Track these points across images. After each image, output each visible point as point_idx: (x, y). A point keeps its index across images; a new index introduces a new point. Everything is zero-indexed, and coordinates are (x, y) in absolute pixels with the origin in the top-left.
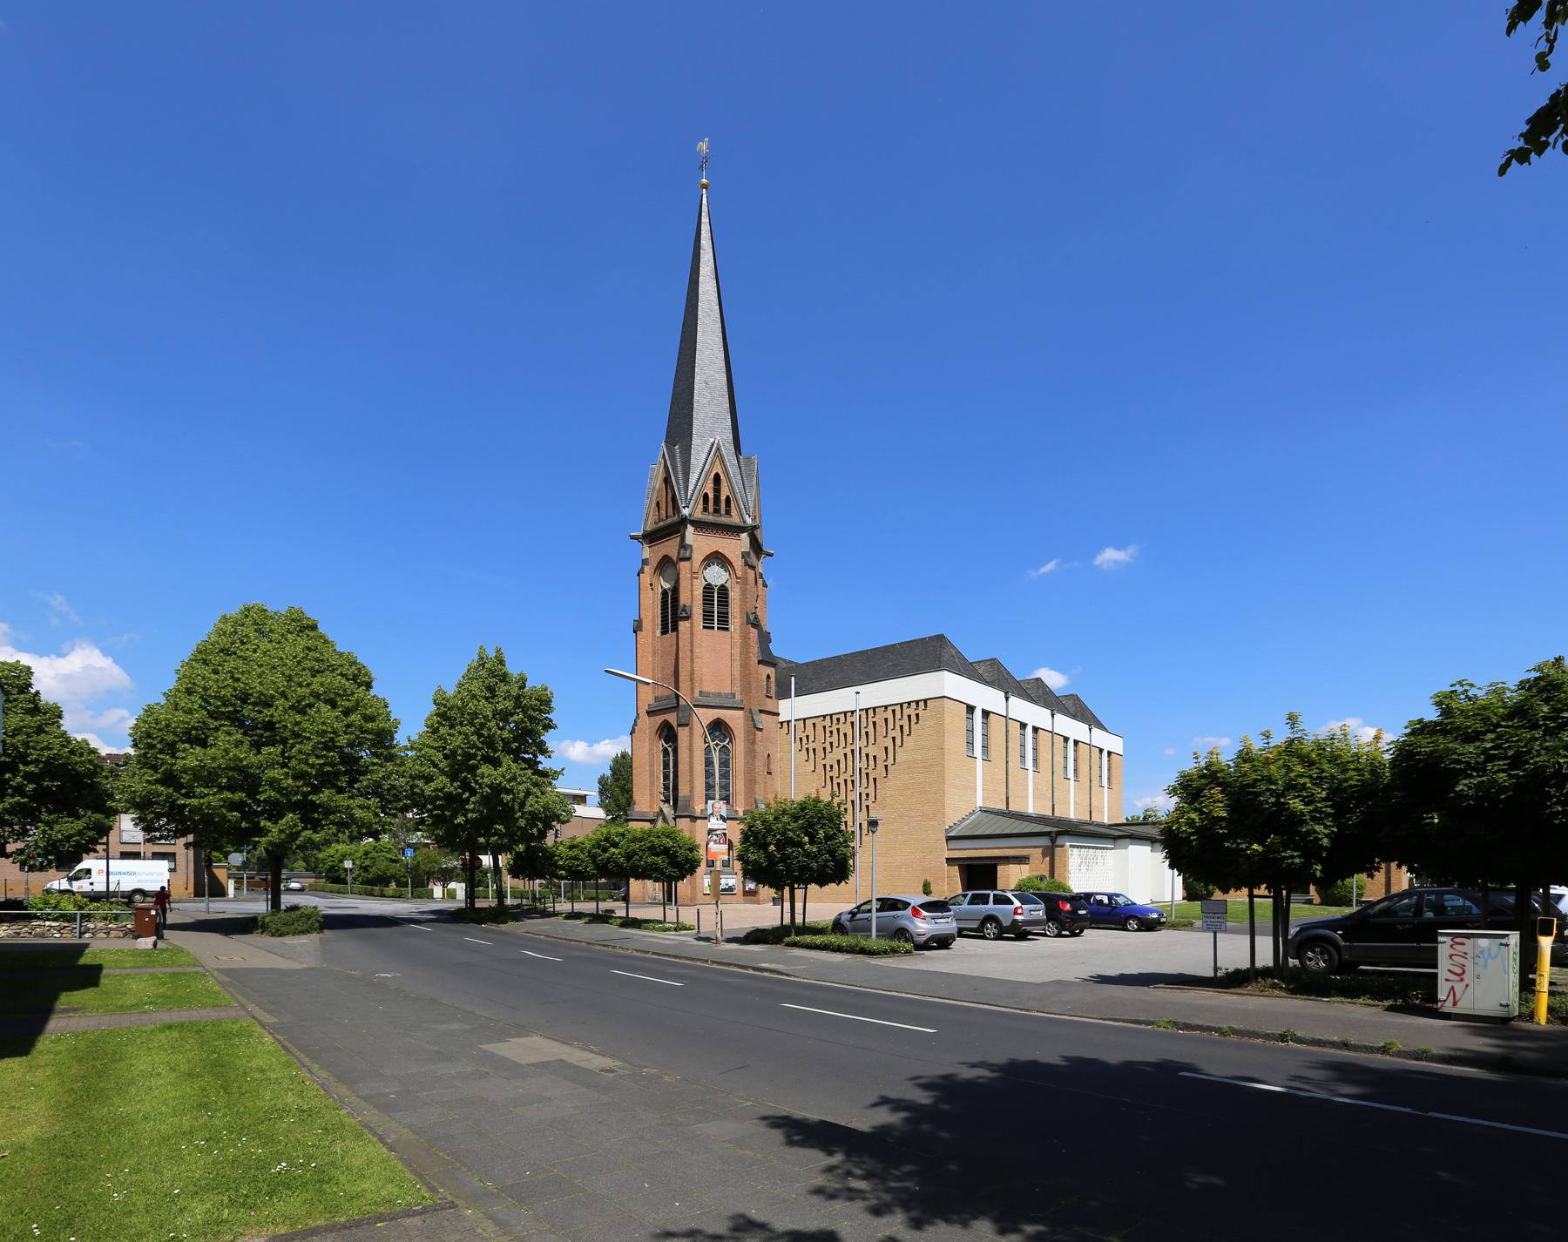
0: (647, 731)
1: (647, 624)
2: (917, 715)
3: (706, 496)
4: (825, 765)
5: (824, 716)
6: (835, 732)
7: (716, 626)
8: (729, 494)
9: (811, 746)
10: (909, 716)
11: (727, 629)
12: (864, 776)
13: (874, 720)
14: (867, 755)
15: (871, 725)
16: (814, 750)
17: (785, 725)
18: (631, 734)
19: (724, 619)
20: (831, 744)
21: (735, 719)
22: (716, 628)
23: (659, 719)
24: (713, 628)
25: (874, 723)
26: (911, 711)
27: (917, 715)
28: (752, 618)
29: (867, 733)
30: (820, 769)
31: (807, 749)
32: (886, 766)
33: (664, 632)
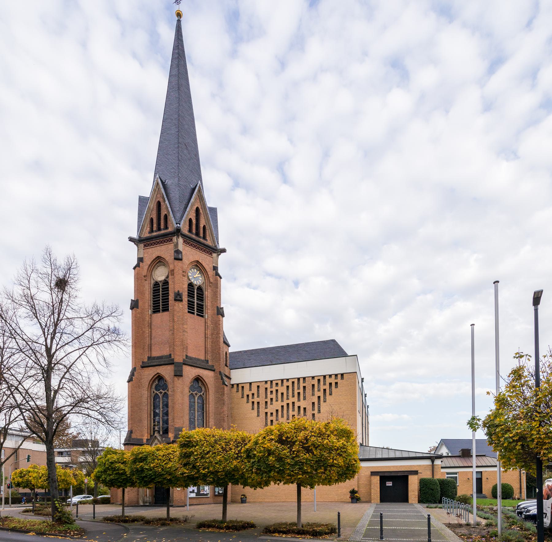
2: (336, 383)
3: (190, 220)
4: (266, 413)
5: (266, 382)
6: (274, 392)
8: (205, 224)
9: (256, 400)
10: (330, 384)
11: (202, 316)
13: (304, 385)
14: (299, 407)
16: (258, 403)
17: (235, 386)
21: (207, 375)
22: (196, 314)
23: (150, 373)
24: (193, 313)
25: (304, 387)
26: (332, 380)
27: (336, 383)
29: (299, 393)
30: (262, 415)
31: (253, 403)
32: (313, 415)
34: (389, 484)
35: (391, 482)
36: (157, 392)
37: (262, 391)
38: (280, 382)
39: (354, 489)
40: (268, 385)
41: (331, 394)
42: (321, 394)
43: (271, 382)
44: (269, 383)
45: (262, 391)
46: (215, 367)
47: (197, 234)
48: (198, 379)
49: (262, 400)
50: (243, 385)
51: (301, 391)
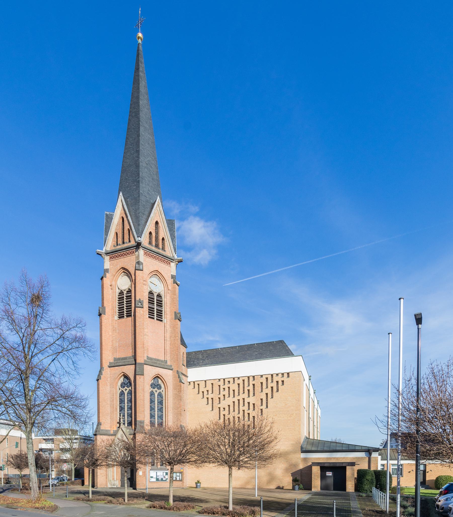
0: (109, 379)
1: (108, 310)
2: (283, 381)
3: (150, 233)
6: (227, 389)
7: (155, 317)
9: (210, 396)
10: (277, 382)
11: (161, 321)
12: (246, 415)
14: (249, 403)
15: (251, 386)
17: (192, 383)
18: (98, 380)
19: (160, 314)
20: (224, 395)
21: (168, 375)
24: (153, 318)
25: (254, 385)
26: (279, 379)
27: (283, 381)
28: (178, 316)
33: (121, 316)
34: (329, 474)
35: (331, 473)
36: (123, 389)
37: (216, 388)
38: (232, 380)
39: (296, 478)
40: (221, 383)
41: (278, 391)
42: (269, 391)
43: (224, 380)
44: (222, 381)
45: (216, 388)
46: (173, 367)
47: (157, 246)
48: (157, 377)
49: (215, 396)
50: (198, 382)
51: (251, 388)
